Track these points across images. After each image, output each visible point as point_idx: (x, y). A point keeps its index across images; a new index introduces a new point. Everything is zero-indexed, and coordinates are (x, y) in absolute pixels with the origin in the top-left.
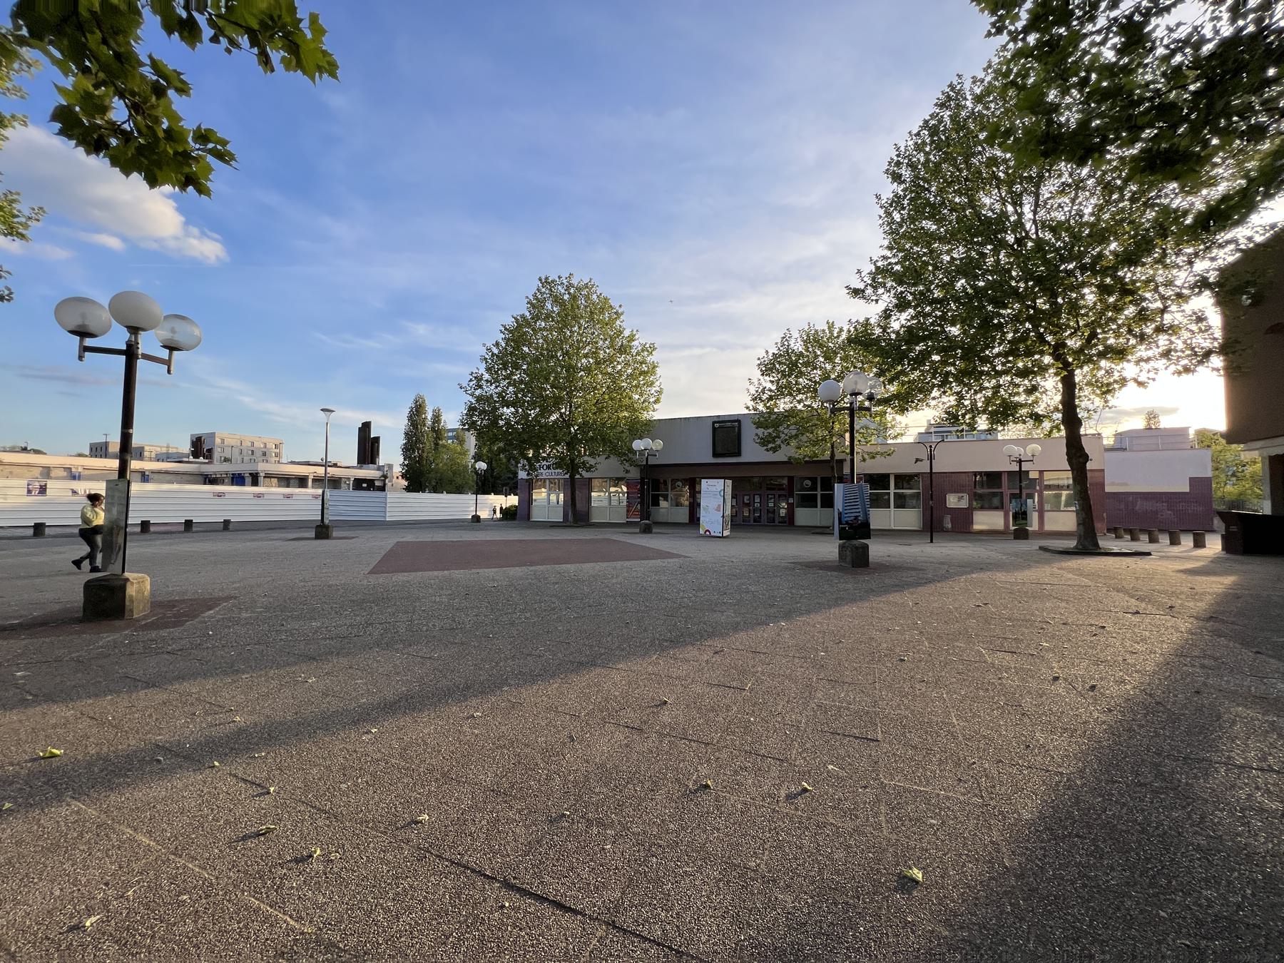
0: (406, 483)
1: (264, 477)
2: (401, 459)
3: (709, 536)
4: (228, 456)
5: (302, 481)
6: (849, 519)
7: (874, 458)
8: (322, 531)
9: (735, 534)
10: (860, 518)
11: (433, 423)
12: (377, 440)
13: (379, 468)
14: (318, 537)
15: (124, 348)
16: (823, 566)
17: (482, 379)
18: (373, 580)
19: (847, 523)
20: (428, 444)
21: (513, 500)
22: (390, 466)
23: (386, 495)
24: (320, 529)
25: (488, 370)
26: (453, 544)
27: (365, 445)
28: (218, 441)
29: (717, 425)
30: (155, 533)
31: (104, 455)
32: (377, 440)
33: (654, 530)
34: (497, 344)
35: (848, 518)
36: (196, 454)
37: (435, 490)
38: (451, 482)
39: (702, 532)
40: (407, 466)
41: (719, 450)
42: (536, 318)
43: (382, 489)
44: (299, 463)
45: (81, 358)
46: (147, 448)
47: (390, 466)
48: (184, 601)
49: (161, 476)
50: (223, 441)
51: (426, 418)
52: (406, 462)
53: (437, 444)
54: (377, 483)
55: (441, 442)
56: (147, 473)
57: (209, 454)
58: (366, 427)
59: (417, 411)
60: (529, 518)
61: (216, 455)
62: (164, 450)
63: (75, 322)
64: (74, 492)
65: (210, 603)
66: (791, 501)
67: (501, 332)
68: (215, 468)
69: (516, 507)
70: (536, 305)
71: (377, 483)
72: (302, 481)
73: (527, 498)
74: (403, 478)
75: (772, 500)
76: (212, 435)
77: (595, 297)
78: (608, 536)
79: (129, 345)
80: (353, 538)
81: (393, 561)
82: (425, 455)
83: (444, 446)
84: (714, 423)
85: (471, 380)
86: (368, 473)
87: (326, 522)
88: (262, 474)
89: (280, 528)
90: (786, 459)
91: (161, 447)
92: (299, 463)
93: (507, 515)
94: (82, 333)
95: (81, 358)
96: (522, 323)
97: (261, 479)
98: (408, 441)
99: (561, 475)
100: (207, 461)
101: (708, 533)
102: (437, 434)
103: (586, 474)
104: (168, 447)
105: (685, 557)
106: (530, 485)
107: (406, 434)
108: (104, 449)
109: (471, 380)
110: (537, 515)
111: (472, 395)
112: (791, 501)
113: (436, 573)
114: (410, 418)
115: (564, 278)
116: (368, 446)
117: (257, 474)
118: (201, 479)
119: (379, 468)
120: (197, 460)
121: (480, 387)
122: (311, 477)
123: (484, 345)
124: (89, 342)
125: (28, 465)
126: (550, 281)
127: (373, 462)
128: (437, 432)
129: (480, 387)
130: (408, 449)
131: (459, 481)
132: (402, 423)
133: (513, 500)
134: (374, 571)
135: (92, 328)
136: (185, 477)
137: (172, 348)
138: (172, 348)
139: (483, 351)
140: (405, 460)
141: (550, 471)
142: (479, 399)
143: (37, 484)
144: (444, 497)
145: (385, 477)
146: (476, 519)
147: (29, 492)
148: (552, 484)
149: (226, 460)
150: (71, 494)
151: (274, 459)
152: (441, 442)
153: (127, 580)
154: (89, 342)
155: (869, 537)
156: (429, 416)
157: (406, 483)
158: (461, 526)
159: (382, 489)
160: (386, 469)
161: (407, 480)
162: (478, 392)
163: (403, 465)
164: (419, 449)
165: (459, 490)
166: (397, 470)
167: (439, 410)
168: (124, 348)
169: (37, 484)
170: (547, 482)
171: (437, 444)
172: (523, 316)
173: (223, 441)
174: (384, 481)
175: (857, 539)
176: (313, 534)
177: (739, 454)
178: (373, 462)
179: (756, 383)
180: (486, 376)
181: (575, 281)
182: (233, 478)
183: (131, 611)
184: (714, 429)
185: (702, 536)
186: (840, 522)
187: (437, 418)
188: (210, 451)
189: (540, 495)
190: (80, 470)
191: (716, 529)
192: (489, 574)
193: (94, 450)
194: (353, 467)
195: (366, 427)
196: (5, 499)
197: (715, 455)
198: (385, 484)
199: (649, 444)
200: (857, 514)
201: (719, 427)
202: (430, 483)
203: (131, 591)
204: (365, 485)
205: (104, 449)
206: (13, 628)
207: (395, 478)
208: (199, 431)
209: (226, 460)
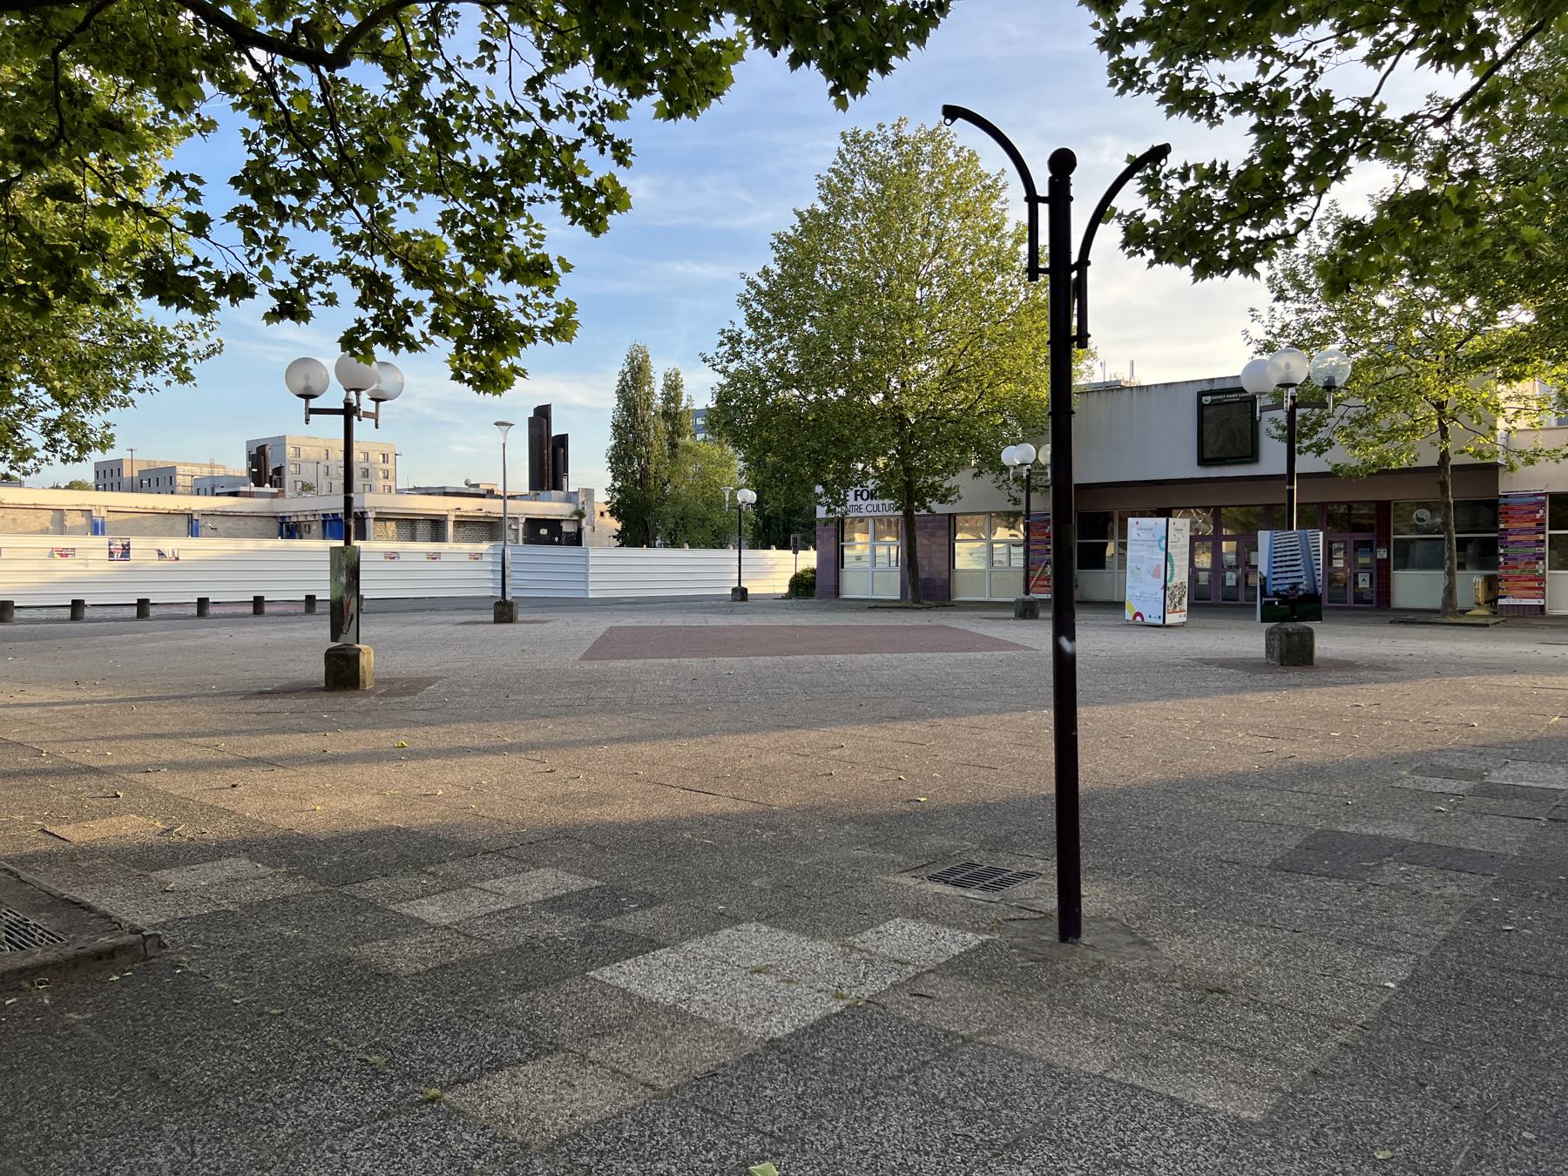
0: (619, 526)
1: (376, 519)
2: (606, 478)
3: (1140, 623)
4: (311, 480)
5: (436, 527)
6: (1281, 588)
7: (1531, 462)
8: (504, 611)
9: (1198, 621)
10: (1301, 587)
11: (667, 401)
12: (563, 440)
13: (570, 498)
14: (498, 620)
15: (342, 406)
16: (1246, 666)
17: (739, 341)
18: (587, 665)
19: (1276, 594)
20: (658, 430)
21: (808, 559)
22: (589, 493)
23: (587, 552)
24: (500, 608)
25: (753, 320)
26: (689, 629)
27: (542, 452)
28: (290, 451)
29: (1207, 400)
30: (216, 617)
31: (108, 487)
32: (563, 440)
33: (1041, 615)
34: (766, 273)
35: (1282, 585)
36: (258, 479)
37: (673, 542)
38: (703, 521)
39: (1129, 616)
40: (619, 491)
41: (1208, 455)
42: (839, 209)
43: (576, 539)
44: (428, 492)
45: (307, 421)
46: (179, 469)
47: (589, 493)
48: (399, 679)
49: (230, 523)
50: (298, 449)
51: (651, 393)
52: (619, 484)
53: (674, 446)
54: (567, 528)
55: (680, 441)
56: (195, 517)
57: (277, 477)
58: (542, 416)
59: (636, 375)
60: (837, 593)
61: (288, 479)
62: (206, 472)
63: (300, 385)
64: (161, 554)
65: (430, 682)
66: (1382, 554)
67: (773, 247)
68: (292, 504)
69: (814, 571)
70: (836, 189)
71: (567, 528)
72: (436, 527)
73: (833, 556)
74: (612, 513)
75: (1341, 554)
76: (281, 440)
77: (950, 154)
78: (944, 623)
79: (348, 404)
80: (546, 622)
81: (604, 647)
82: (652, 468)
83: (688, 449)
84: (1201, 394)
85: (722, 344)
86: (550, 507)
87: (508, 598)
88: (371, 515)
89: (431, 610)
90: (1329, 469)
91: (201, 466)
92: (428, 492)
93: (798, 587)
94: (307, 396)
95: (307, 421)
96: (813, 224)
97: (370, 524)
98: (621, 440)
99: (886, 507)
100: (275, 490)
101: (1138, 618)
102: (674, 425)
103: (936, 507)
104: (212, 466)
105: (1026, 648)
106: (839, 528)
107: (616, 427)
108: (115, 473)
109: (722, 344)
110: (854, 585)
111: (724, 371)
112: (1382, 554)
113: (661, 661)
114: (622, 392)
115: (888, 127)
116: (548, 452)
117: (362, 513)
118: (274, 525)
119: (570, 498)
120: (261, 489)
121: (738, 356)
122: (452, 518)
123: (743, 275)
124: (314, 404)
125: (36, 508)
126: (861, 137)
127: (557, 486)
128: (673, 417)
129: (738, 356)
130: (621, 457)
131: (718, 519)
132: (610, 403)
133: (808, 559)
134: (585, 658)
135: (315, 387)
136: (251, 522)
137: (378, 401)
138: (378, 401)
139: (743, 287)
140: (615, 479)
141: (875, 502)
142: (736, 378)
143: (119, 542)
144: (685, 555)
145: (581, 514)
146: (741, 594)
147: (111, 554)
148: (877, 528)
149: (307, 488)
150: (156, 556)
151: (382, 482)
152: (680, 441)
153: (359, 650)
154: (314, 404)
155: (1318, 617)
156: (658, 387)
157: (619, 526)
158: (715, 607)
159: (576, 539)
160: (581, 500)
161: (620, 518)
162: (732, 368)
163: (612, 489)
164: (640, 457)
165: (717, 540)
166: (602, 498)
167: (677, 374)
168: (342, 406)
169: (119, 542)
170: (871, 522)
171: (674, 446)
172: (813, 213)
173: (298, 449)
174: (579, 522)
175: (1294, 620)
176: (492, 618)
177: (1252, 456)
178: (557, 486)
179: (1266, 318)
180: (749, 334)
181: (908, 131)
182: (324, 522)
183: (364, 682)
184: (1201, 407)
185: (1128, 624)
186: (1264, 594)
187: (673, 390)
188: (279, 471)
189: (859, 546)
190: (104, 513)
191: (1152, 614)
192: (726, 663)
193: (101, 474)
194: (522, 497)
195: (542, 416)
196: (86, 565)
197: (1203, 461)
198: (580, 530)
199: (1029, 453)
200: (1299, 580)
201: (1213, 404)
202: (663, 524)
203: (363, 661)
204: (544, 532)
205: (115, 473)
206: (269, 692)
207: (598, 514)
208: (262, 433)
209: (307, 488)
